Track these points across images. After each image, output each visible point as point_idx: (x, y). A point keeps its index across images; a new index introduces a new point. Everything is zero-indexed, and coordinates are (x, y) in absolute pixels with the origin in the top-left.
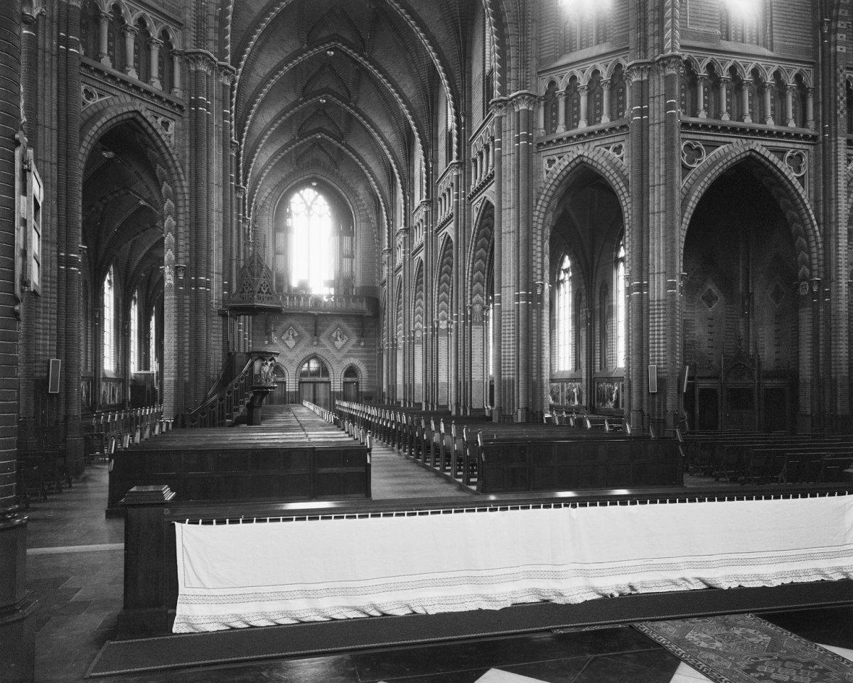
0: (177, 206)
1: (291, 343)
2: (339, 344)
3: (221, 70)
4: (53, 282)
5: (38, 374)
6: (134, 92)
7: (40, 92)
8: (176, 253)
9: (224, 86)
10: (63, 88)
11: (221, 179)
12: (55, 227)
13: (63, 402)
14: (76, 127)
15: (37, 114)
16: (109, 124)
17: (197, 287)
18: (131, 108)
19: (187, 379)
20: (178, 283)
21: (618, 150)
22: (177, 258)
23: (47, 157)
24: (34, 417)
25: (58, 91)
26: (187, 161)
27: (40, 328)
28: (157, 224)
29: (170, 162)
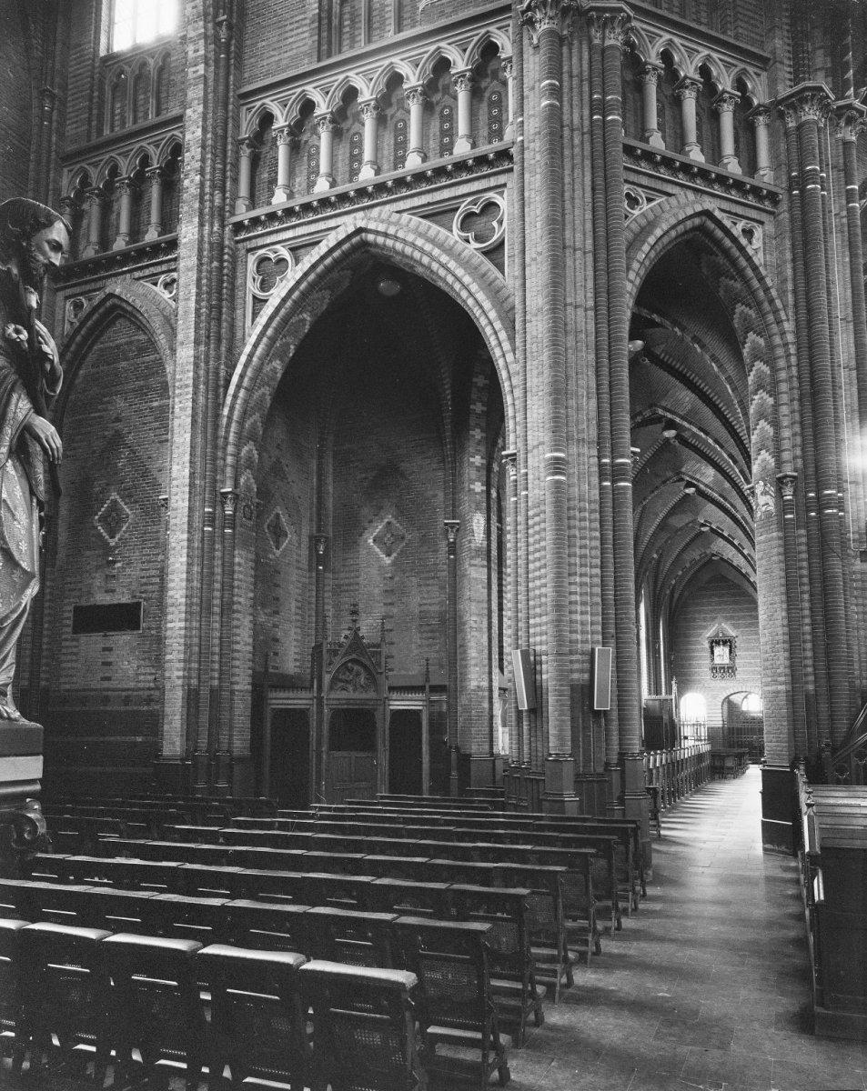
0: (774, 370)
3: (840, 117)
4: (594, 511)
5: (576, 676)
6: (699, 185)
7: (567, 195)
8: (777, 454)
9: (846, 144)
10: (600, 181)
11: (850, 310)
12: (593, 414)
13: (614, 726)
14: (621, 242)
15: (564, 230)
16: (665, 240)
17: (820, 511)
18: (699, 208)
19: (811, 687)
20: (783, 507)
22: (779, 463)
23: (580, 299)
24: (571, 755)
25: (593, 189)
26: (790, 286)
27: (576, 593)
28: (683, 470)
29: (761, 294)
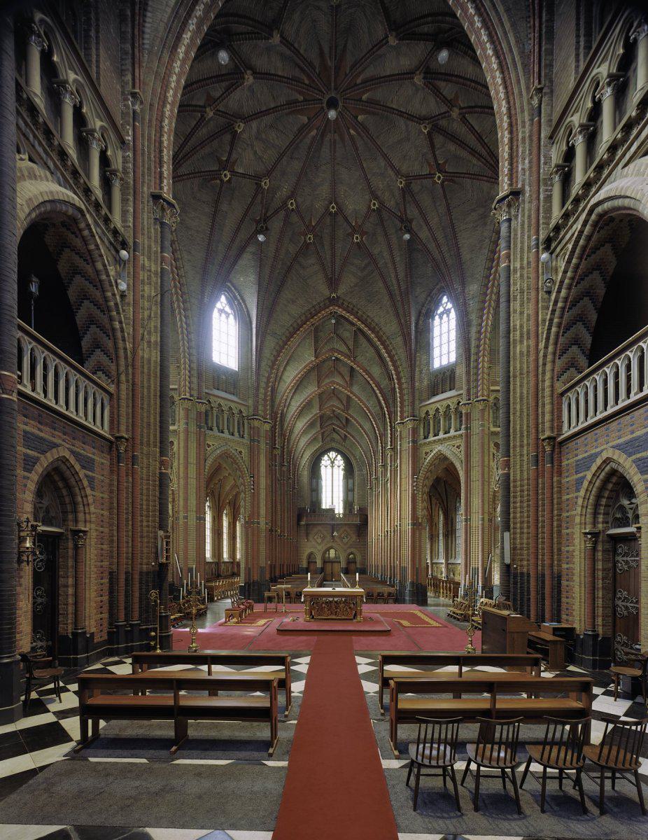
0: (245, 488)
1: (319, 540)
2: (345, 540)
21: (458, 447)
